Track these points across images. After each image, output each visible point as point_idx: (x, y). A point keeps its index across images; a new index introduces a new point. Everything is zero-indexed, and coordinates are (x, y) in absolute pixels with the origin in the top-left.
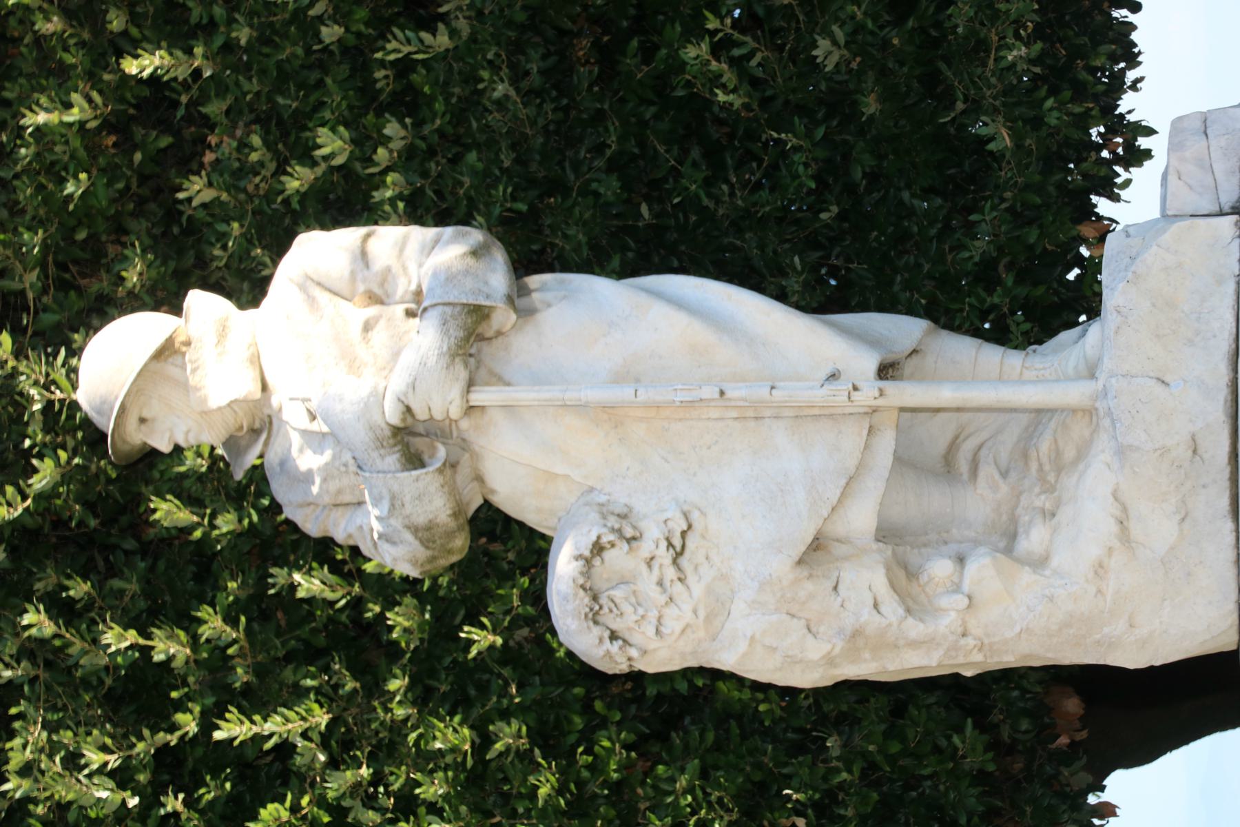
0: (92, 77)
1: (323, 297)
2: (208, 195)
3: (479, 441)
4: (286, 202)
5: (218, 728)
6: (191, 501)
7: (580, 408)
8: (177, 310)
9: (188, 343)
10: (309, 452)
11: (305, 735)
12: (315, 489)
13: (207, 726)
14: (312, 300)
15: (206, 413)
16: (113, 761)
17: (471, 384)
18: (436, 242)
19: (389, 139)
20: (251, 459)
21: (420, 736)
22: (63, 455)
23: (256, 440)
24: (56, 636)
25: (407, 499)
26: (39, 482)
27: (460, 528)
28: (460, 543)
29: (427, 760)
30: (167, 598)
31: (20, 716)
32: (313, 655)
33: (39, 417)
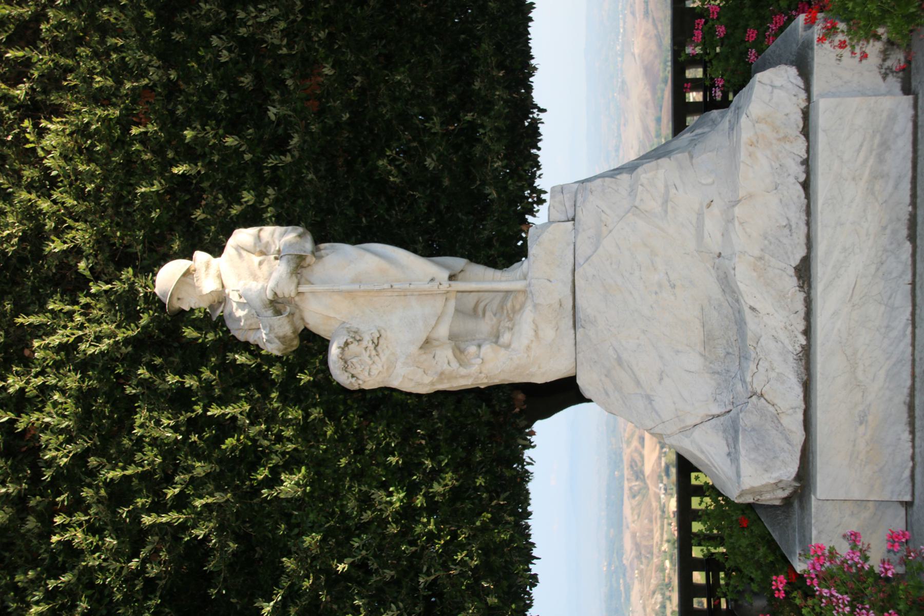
1: (244, 253)
2: (203, 216)
3: (302, 305)
4: (231, 218)
5: (209, 411)
6: (198, 329)
7: (340, 292)
8: (191, 258)
9: (195, 271)
10: (240, 310)
11: (241, 413)
12: (242, 324)
13: (205, 410)
14: (240, 255)
15: (202, 296)
16: (172, 423)
17: (299, 284)
18: (285, 233)
19: (269, 195)
20: (218, 313)
21: (283, 414)
22: (151, 312)
23: (220, 306)
24: (150, 378)
25: (276, 326)
27: (296, 337)
28: (296, 343)
29: (286, 422)
30: (190, 364)
31: (139, 407)
32: (244, 385)
33: (142, 298)
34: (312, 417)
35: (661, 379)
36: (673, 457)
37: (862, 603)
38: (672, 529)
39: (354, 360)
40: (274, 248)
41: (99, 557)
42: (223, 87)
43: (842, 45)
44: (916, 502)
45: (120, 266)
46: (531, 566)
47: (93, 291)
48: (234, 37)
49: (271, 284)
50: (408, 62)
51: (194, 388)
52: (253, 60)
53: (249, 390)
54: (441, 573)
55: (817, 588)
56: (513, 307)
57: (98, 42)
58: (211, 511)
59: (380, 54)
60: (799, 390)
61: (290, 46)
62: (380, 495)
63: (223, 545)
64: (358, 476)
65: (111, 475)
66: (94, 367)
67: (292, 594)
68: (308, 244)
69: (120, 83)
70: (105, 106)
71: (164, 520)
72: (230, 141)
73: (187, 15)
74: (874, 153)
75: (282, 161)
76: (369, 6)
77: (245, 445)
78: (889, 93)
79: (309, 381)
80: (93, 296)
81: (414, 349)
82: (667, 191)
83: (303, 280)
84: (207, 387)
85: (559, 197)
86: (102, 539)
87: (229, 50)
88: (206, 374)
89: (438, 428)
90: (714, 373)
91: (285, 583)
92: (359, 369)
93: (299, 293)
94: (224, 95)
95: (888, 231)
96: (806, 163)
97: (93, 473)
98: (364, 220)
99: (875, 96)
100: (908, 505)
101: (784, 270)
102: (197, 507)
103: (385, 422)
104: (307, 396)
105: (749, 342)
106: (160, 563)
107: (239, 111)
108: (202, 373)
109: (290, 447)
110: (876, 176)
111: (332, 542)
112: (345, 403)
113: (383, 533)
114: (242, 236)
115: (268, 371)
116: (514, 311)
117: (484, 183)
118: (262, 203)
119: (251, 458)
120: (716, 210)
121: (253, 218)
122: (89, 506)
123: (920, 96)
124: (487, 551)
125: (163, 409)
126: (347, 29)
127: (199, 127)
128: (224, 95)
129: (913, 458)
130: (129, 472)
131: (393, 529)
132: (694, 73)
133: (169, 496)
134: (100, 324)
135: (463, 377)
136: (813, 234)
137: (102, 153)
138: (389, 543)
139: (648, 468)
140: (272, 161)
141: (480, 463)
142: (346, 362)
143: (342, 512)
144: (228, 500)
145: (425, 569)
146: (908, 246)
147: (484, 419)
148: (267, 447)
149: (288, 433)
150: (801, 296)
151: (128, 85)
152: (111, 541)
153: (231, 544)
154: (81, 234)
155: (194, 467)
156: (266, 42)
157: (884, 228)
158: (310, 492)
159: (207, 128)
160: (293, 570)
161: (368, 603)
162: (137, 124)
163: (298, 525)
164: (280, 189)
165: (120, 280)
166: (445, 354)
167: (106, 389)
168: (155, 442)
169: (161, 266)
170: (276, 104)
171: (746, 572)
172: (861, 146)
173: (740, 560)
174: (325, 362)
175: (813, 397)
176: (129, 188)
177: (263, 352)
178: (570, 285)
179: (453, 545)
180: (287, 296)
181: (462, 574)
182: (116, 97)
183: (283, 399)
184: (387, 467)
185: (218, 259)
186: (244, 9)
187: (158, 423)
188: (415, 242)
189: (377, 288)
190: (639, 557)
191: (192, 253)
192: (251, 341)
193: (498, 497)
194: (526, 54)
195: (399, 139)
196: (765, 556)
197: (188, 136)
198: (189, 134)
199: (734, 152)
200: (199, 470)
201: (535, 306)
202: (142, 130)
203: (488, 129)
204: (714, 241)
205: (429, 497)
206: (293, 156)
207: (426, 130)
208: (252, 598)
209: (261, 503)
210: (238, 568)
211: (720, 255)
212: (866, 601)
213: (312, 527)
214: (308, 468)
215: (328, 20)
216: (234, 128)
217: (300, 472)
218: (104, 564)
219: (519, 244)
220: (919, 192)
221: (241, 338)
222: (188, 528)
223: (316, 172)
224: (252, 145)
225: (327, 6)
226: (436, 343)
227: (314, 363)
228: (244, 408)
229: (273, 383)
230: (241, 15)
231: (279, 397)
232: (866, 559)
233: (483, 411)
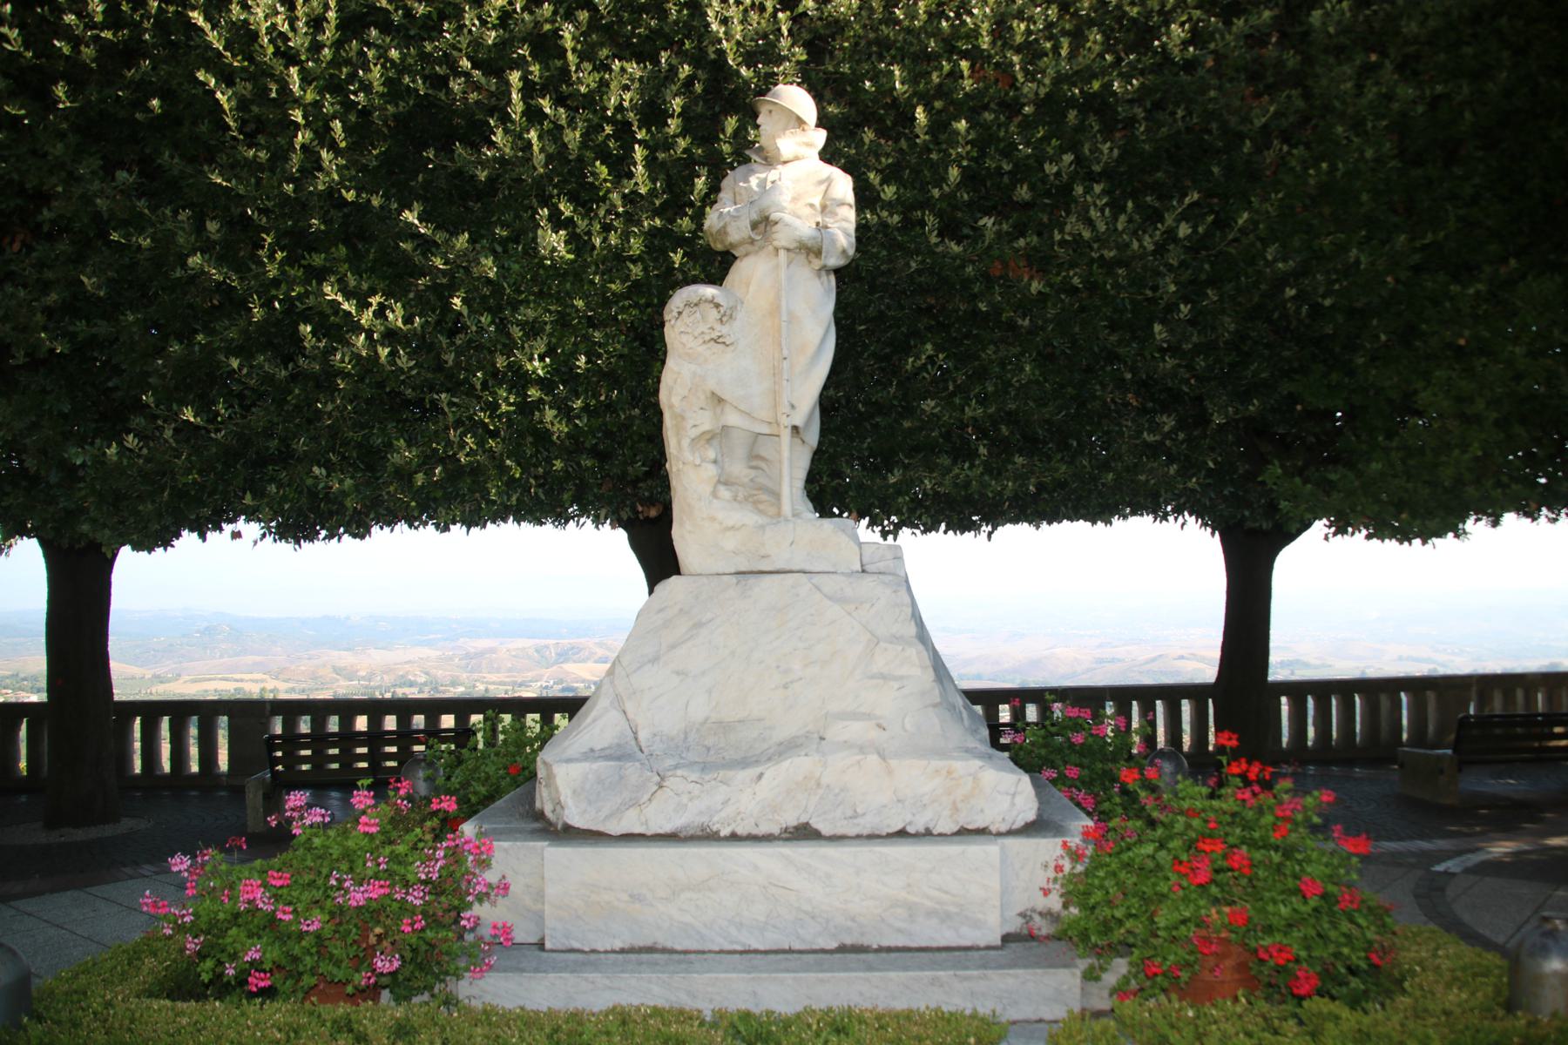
1: (823, 187)
2: (867, 140)
4: (864, 173)
6: (736, 133)
7: (778, 298)
8: (818, 126)
11: (636, 184)
13: (640, 142)
14: (821, 182)
15: (774, 138)
16: (626, 104)
17: (788, 250)
18: (847, 234)
20: (754, 157)
26: (743, 71)
28: (719, 247)
29: (626, 236)
31: (645, 67)
32: (670, 186)
34: (632, 266)
35: (678, 673)
36: (587, 694)
37: (430, 893)
38: (499, 692)
39: (698, 315)
40: (829, 221)
41: (474, 25)
42: (1016, 165)
43: (1058, 868)
44: (545, 955)
45: (808, 46)
46: (459, 525)
47: (780, 15)
48: (1073, 178)
49: (787, 217)
50: (1046, 380)
51: (667, 129)
52: (1047, 201)
53: (664, 193)
54: (451, 418)
55: (444, 844)
56: (761, 502)
57: (1063, 28)
58: (522, 150)
59: (1054, 347)
60: (667, 828)
61: (1063, 243)
62: (540, 346)
63: (484, 164)
64: (563, 322)
65: (567, 35)
66: (691, 16)
67: (426, 245)
68: (835, 261)
69: (1018, 50)
70: (992, 32)
71: (514, 96)
72: (954, 173)
73: (1096, 128)
74: (937, 906)
75: (931, 232)
76: (1109, 335)
77: (599, 189)
78: (1004, 920)
79: (674, 263)
80: (774, 15)
81: (711, 385)
82: (896, 678)
83: (792, 255)
84: (668, 144)
85: (889, 555)
86: (494, 27)
87: (1058, 174)
88: (682, 143)
89: (618, 415)
90: (686, 733)
91: (440, 237)
92: (688, 320)
94: (1007, 167)
95: (849, 923)
97: (569, 16)
98: (863, 327)
99: (1002, 905)
100: (541, 945)
101: (805, 810)
102: (528, 133)
103: (626, 351)
104: (655, 260)
105: (722, 773)
106: (465, 93)
107: (989, 184)
108: (684, 138)
109: (597, 241)
110: (912, 910)
111: (486, 291)
112: (648, 305)
113: (496, 351)
114: (843, 185)
115: (686, 214)
116: (755, 503)
117: (906, 467)
118: (882, 209)
119: (584, 196)
120: (874, 734)
121: (865, 197)
122: (531, 13)
123: (1000, 952)
124: (475, 471)
125: (642, 95)
126: (1083, 309)
127: (970, 137)
128: (1007, 167)
129: (593, 951)
130: (570, 56)
131: (501, 362)
132: (1032, 713)
133: (541, 101)
134: (742, 22)
135: (679, 443)
136: (846, 842)
137: (939, 29)
138: (485, 358)
139: (571, 667)
140: (931, 220)
141: (578, 464)
142: (696, 305)
143: (521, 302)
144: (535, 169)
145: (455, 400)
146: (834, 945)
147: (630, 468)
148: (596, 214)
149: (613, 240)
150: (776, 830)
151: (1015, 59)
152: (491, 37)
153: (485, 173)
155: (574, 129)
156: (1068, 215)
157: (853, 920)
158: (544, 265)
159: (969, 147)
160: (453, 247)
161: (415, 334)
162: (972, 67)
163: (505, 251)
164: (898, 229)
165: (792, 46)
166: (704, 421)
167: (667, 29)
168: (604, 85)
169: (809, 91)
170: (997, 227)
171: (457, 771)
172: (946, 892)
173: (471, 764)
174: (695, 281)
175: (660, 843)
176: (899, 58)
177: (708, 209)
178: (788, 568)
180: (774, 236)
181: (449, 443)
182: (1003, 45)
183: (653, 233)
184: (574, 355)
185: (817, 157)
186: (1104, 192)
187: (626, 88)
188: (837, 388)
189: (783, 343)
190: (468, 656)
191: (824, 128)
192: (721, 195)
193: (539, 486)
194: (1054, 517)
195: (956, 369)
196: (475, 793)
197: (959, 125)
198: (962, 125)
199: (943, 754)
200: (571, 135)
201: (762, 527)
202: (966, 73)
203: (969, 473)
204: (842, 731)
206: (937, 245)
207: (967, 400)
208: (423, 199)
209: (532, 208)
210: (457, 182)
211: (822, 739)
212: (433, 897)
213: (503, 267)
214: (573, 262)
215: (1092, 287)
216: (969, 177)
217: (568, 252)
218: (465, 31)
219: (836, 510)
220: (893, 955)
221: (725, 183)
222: (504, 123)
223: (919, 272)
224: (949, 197)
225: (1108, 287)
226: (718, 410)
227: (695, 269)
228: (641, 186)
229: (672, 221)
230: (1098, 188)
231: (655, 227)
232: (480, 901)
233: (639, 468)
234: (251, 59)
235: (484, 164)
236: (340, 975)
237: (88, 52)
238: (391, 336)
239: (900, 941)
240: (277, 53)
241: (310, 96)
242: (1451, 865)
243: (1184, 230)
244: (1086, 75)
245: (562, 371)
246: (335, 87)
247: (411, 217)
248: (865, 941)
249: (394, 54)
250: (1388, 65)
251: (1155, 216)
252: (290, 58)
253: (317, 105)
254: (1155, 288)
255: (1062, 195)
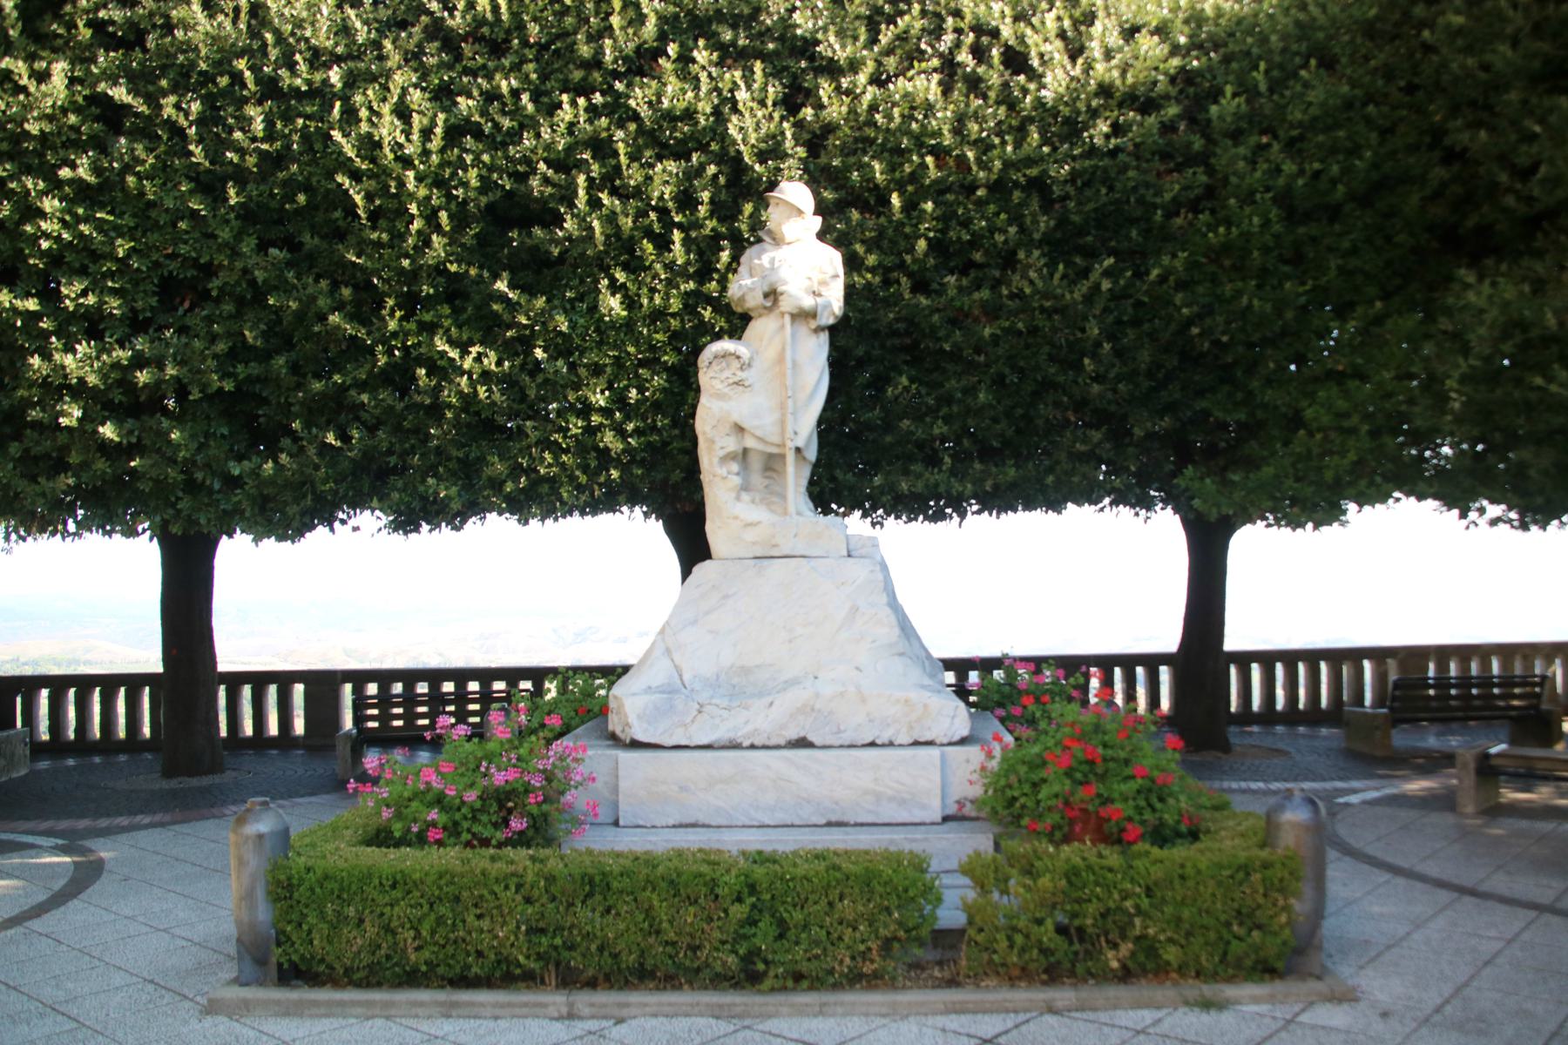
0: (889, 182)
6: (751, 216)
7: (783, 349)
20: (765, 238)
26: (757, 167)
28: (739, 310)
29: (667, 297)
32: (700, 253)
35: (711, 632)
48: (1019, 244)
60: (705, 741)
66: (717, 121)
72: (922, 245)
78: (944, 805)
84: (698, 225)
87: (1006, 242)
93: (783, 314)
96: (891, 744)
97: (621, 125)
100: (616, 824)
109: (645, 301)
110: (878, 797)
124: (552, 481)
126: (1027, 347)
150: (783, 742)
154: (836, 110)
166: (731, 444)
168: (649, 178)
179: (557, 449)
184: (627, 388)
198: (929, 206)
205: (600, 427)
234: (373, 160)
235: (558, 242)
236: (486, 834)
237: (251, 161)
238: (486, 376)
239: (870, 819)
240: (397, 159)
241: (422, 192)
242: (1354, 799)
243: (1106, 285)
244: (1030, 161)
245: (620, 400)
246: (439, 183)
247: (501, 286)
248: (845, 819)
249: (486, 158)
250: (1276, 147)
251: (1085, 273)
252: (406, 162)
253: (428, 198)
254: (1083, 330)
255: (1008, 260)
